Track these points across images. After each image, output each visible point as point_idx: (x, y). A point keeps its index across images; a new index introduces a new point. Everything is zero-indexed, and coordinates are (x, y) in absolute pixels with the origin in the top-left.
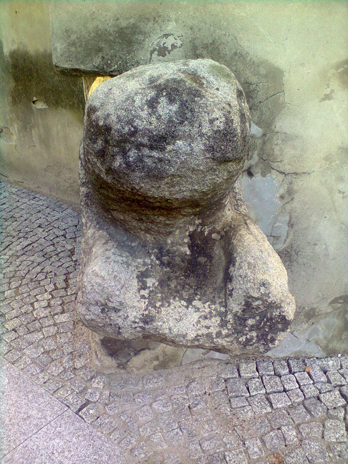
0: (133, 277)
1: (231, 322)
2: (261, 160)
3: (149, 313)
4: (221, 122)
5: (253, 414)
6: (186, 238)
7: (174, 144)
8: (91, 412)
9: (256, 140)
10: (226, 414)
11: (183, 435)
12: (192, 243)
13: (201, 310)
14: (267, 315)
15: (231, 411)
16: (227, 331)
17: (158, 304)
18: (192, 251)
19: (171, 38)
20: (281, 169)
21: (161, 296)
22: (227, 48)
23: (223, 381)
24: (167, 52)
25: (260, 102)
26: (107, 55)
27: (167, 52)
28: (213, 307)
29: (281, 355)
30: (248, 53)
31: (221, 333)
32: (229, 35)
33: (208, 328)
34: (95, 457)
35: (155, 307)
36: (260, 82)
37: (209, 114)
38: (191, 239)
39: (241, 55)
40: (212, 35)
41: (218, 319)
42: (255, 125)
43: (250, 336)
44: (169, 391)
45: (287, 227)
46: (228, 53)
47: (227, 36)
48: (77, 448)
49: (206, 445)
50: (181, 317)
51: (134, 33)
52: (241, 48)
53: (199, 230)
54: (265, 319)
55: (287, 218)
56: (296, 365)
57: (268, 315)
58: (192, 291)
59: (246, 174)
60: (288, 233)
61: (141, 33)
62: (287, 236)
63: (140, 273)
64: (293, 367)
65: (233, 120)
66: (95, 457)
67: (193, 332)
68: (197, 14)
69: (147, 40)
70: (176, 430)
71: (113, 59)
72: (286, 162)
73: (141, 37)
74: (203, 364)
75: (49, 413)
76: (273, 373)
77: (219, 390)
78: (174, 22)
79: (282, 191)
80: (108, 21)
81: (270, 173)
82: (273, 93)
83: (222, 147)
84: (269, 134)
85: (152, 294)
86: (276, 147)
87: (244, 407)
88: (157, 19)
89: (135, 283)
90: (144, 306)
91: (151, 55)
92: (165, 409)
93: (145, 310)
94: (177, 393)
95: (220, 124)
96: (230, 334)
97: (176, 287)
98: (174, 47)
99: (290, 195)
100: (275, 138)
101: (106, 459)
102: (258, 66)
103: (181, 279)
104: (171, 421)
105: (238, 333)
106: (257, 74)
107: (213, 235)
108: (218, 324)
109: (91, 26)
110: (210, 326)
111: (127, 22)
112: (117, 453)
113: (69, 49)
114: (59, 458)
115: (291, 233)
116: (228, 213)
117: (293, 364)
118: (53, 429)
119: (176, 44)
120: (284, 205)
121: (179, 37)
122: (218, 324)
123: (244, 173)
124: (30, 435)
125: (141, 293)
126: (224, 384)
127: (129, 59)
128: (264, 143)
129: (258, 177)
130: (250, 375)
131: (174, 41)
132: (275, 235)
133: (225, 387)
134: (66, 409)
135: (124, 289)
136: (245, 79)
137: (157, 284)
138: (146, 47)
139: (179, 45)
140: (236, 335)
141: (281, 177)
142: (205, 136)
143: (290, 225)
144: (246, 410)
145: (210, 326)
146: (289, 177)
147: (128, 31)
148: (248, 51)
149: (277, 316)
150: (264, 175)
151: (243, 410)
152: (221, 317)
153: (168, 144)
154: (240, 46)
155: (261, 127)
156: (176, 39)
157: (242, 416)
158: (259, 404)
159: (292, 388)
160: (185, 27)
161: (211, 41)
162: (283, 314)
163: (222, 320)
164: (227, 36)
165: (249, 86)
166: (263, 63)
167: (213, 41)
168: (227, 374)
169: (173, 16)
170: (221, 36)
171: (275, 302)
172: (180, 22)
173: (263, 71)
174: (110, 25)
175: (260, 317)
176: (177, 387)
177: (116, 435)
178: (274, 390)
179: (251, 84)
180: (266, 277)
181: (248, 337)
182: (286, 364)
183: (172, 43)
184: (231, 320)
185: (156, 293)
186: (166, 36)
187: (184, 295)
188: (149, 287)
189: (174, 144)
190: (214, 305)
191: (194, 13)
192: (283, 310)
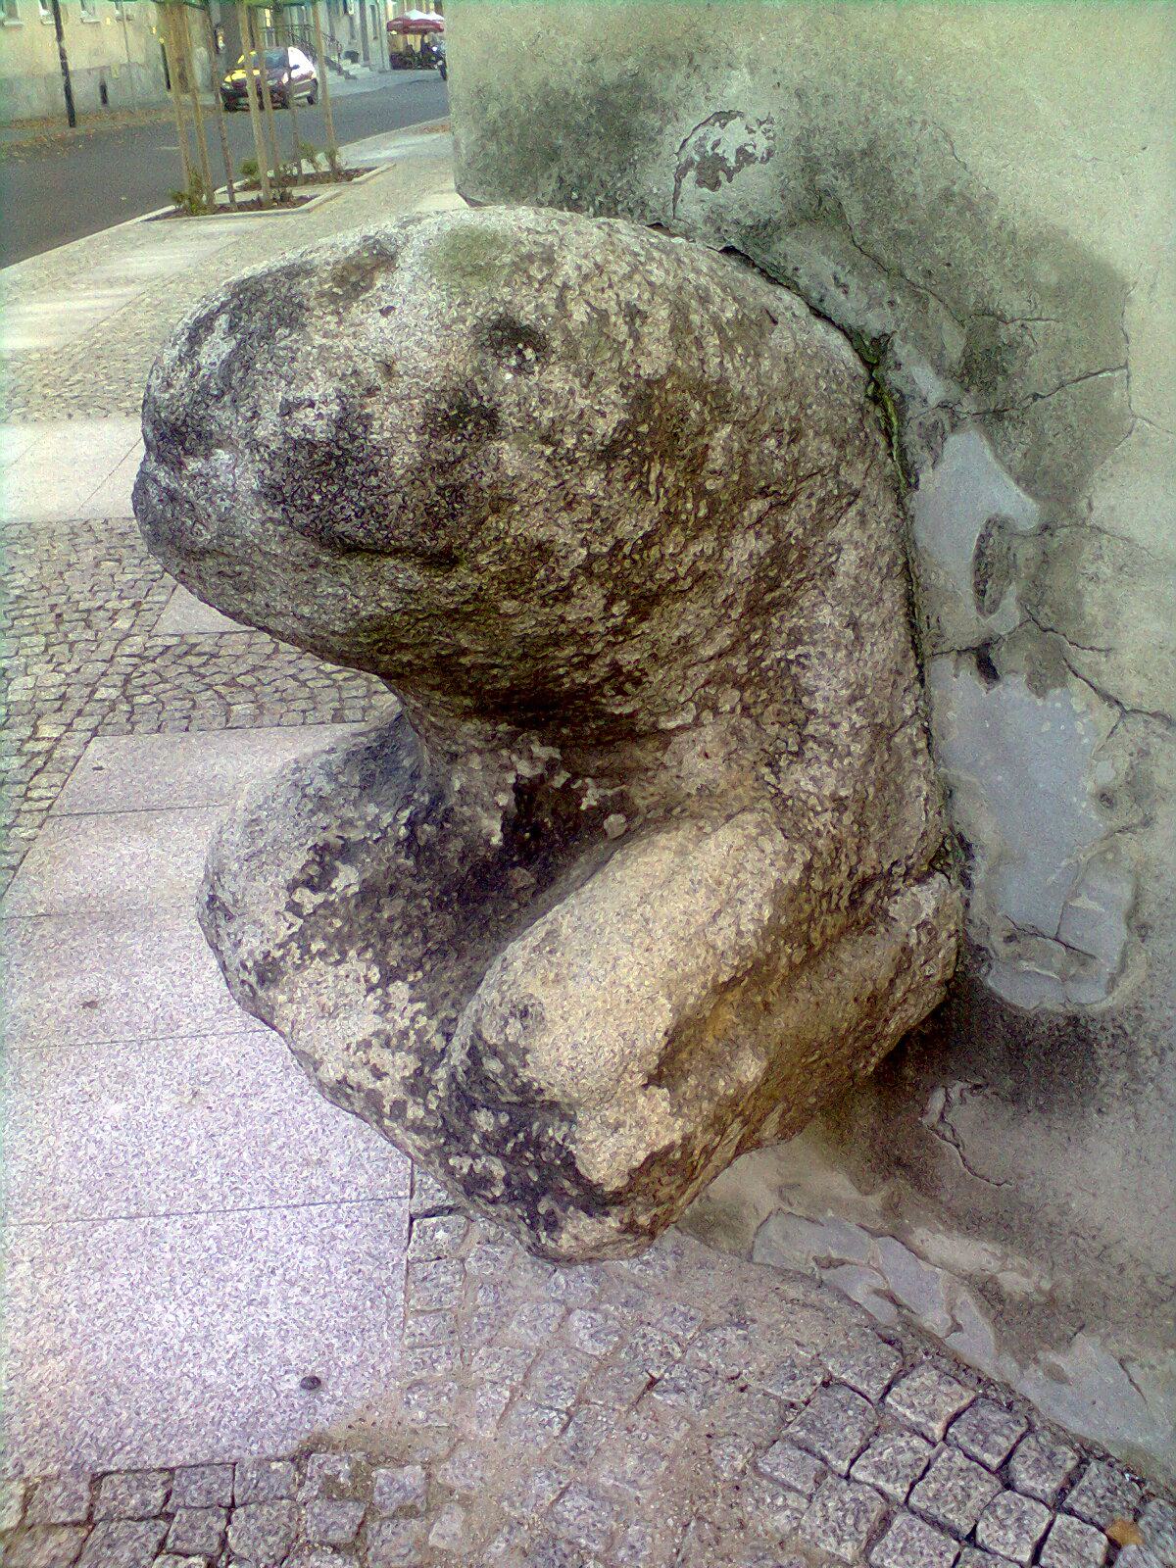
0: (301, 845)
1: (441, 1094)
2: (1030, 625)
3: (283, 958)
4: (320, 416)
5: (788, 1528)
6: (504, 791)
7: (206, 458)
8: (440, 1235)
9: (1016, 542)
10: (718, 1467)
11: (556, 1438)
12: (519, 816)
13: (390, 1015)
14: (531, 1124)
15: (743, 1472)
16: (421, 1113)
17: (317, 946)
18: (506, 838)
19: (735, 124)
20: (1110, 685)
21: (339, 930)
22: (917, 172)
23: (819, 1380)
24: (722, 176)
25: (1036, 396)
26: (570, 171)
27: (722, 176)
28: (423, 1020)
29: (1075, 1425)
30: (990, 197)
31: (405, 1111)
32: (924, 123)
33: (378, 1074)
34: (334, 1341)
35: (305, 950)
36: (1036, 316)
37: (289, 383)
38: (518, 802)
39: (970, 205)
40: (867, 119)
41: (412, 1063)
42: (1012, 483)
43: (484, 1167)
44: (654, 1308)
45: (1123, 927)
46: (920, 190)
47: (918, 127)
48: (324, 1296)
49: (574, 1502)
50: (336, 1006)
51: (634, 108)
52: (966, 176)
53: (559, 781)
54: (521, 1136)
55: (1125, 892)
56: (1100, 1492)
57: (535, 1126)
58: (417, 952)
59: (969, 664)
60: (1124, 955)
61: (654, 105)
62: (1123, 967)
63: (341, 842)
64: (1082, 1492)
65: (369, 417)
66: (334, 1341)
67: (339, 1066)
68: (818, 44)
69: (669, 129)
70: (554, 1414)
71: (582, 187)
72: (1127, 657)
73: (653, 120)
74: (813, 1297)
75: (362, 1180)
76: (994, 1461)
77: (779, 1394)
78: (745, 70)
79: (1107, 773)
80: (570, 64)
81: (1063, 685)
82: (1083, 366)
83: (317, 498)
84: (1065, 530)
85: (321, 912)
86: (1091, 587)
87: (789, 1488)
88: (697, 60)
89: (298, 861)
90: (284, 932)
91: (678, 181)
92: (589, 1344)
93: (280, 946)
94: (667, 1327)
95: (315, 423)
96: (426, 1128)
97: (391, 920)
98: (745, 160)
99: (1137, 799)
100: (1087, 553)
101: (347, 1364)
102: (1031, 252)
103: (419, 907)
104: (566, 1385)
105: (447, 1137)
106: (1026, 283)
107: (612, 818)
108: (403, 1078)
109: (532, 78)
110: (386, 1074)
111: (618, 69)
112: (382, 1368)
113: (483, 147)
114: (271, 1290)
115: (1139, 959)
116: (693, 762)
117: (1097, 1482)
118: (332, 1221)
119: (750, 149)
120: (1111, 833)
121: (761, 123)
122: (403, 1078)
123: (965, 656)
124: (279, 1202)
125: (297, 898)
126: (809, 1391)
127: (620, 189)
128: (1046, 560)
129: (1014, 689)
130: (913, 1418)
131: (746, 138)
132: (1072, 942)
133: (803, 1398)
134: (401, 1194)
135: (254, 863)
136: (980, 296)
137: (356, 889)
138: (665, 155)
139: (760, 152)
140: (442, 1141)
141: (1107, 716)
142: (262, 449)
143: (1134, 923)
144: (780, 1501)
145: (386, 1074)
146: (1137, 728)
147: (619, 98)
148: (992, 188)
149: (553, 1145)
150: (1039, 685)
151: (774, 1497)
152: (422, 1060)
153: (189, 452)
154: (965, 166)
155: (1035, 496)
156: (751, 131)
157: (749, 1509)
158: (841, 1514)
159: (999, 1549)
160: (781, 91)
161: (863, 145)
162: (572, 1147)
163: (418, 1072)
164: (918, 127)
165: (994, 328)
166: (1047, 242)
167: (872, 144)
168: (846, 1367)
169: (742, 50)
170: (897, 126)
171: (541, 1091)
172: (764, 70)
173: (1047, 273)
174: (576, 76)
175: (511, 1120)
176: (682, 1308)
177: (424, 1327)
178: (934, 1511)
179: (1001, 318)
180: (544, 996)
181: (478, 1168)
182: (1070, 1465)
183: (741, 142)
184: (441, 1086)
185: (334, 915)
186: (723, 117)
187: (393, 952)
188: (333, 891)
189: (206, 458)
190: (429, 1018)
191: (808, 40)
192: (577, 1136)
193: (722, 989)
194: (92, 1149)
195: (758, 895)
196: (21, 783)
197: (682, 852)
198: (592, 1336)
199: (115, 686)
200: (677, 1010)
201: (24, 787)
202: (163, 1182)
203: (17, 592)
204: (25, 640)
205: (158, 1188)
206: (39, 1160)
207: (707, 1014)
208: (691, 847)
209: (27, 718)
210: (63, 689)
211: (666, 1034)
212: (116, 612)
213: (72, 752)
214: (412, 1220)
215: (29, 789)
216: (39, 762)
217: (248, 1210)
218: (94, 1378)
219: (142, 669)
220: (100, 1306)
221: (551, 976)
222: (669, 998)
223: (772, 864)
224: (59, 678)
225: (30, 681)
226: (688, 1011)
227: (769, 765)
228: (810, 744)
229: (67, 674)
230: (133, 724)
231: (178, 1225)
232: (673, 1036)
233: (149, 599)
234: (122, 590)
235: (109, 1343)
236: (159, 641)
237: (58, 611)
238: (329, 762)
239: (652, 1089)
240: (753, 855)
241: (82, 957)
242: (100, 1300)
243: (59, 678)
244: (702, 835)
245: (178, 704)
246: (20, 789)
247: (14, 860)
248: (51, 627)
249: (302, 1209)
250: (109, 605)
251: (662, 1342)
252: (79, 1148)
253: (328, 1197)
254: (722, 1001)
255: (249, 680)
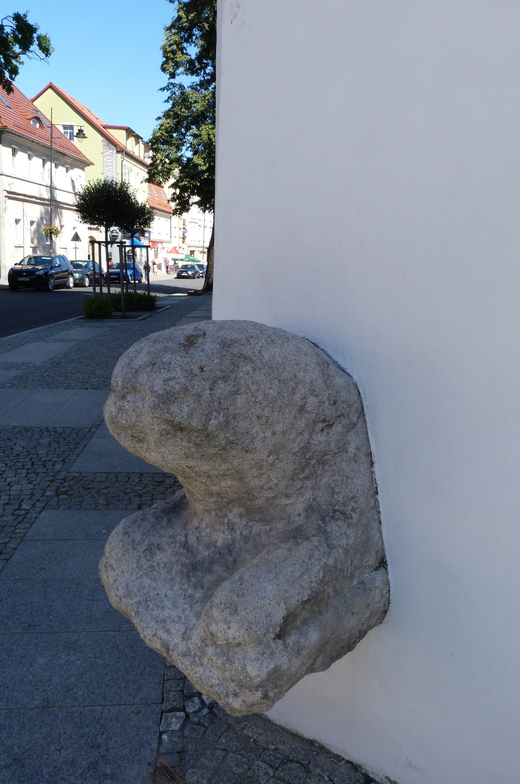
193: (304, 603)
194: (30, 677)
195: (318, 568)
196: (12, 526)
197: (290, 550)
198: (236, 765)
199: (53, 491)
200: (287, 609)
201: (14, 528)
202: (59, 693)
203: (17, 452)
204: (19, 471)
205: (57, 695)
206: (7, 681)
207: (298, 612)
208: (293, 548)
209: (17, 501)
210: (32, 491)
211: (283, 618)
212: (56, 462)
213: (34, 515)
214: (162, 713)
215: (15, 529)
216: (21, 518)
217: (94, 706)
218: (22, 779)
219: (64, 485)
220: (28, 747)
221: (241, 593)
222: (285, 604)
223: (323, 556)
224: (31, 486)
225: (19, 487)
226: (291, 610)
227: (322, 520)
228: (338, 513)
229: (34, 485)
230: (59, 506)
231: (64, 711)
232: (286, 619)
233: (69, 458)
234: (59, 454)
235: (30, 763)
236: (72, 474)
237: (33, 460)
238: (155, 513)
239: (277, 640)
240: (317, 552)
241: (32, 597)
242: (28, 744)
243: (31, 486)
244: (297, 544)
245: (77, 499)
246: (12, 529)
247: (8, 556)
248: (30, 466)
249: (117, 707)
250: (53, 460)
251: (265, 769)
252: (25, 677)
253: (127, 702)
254: (303, 608)
255: (105, 491)
